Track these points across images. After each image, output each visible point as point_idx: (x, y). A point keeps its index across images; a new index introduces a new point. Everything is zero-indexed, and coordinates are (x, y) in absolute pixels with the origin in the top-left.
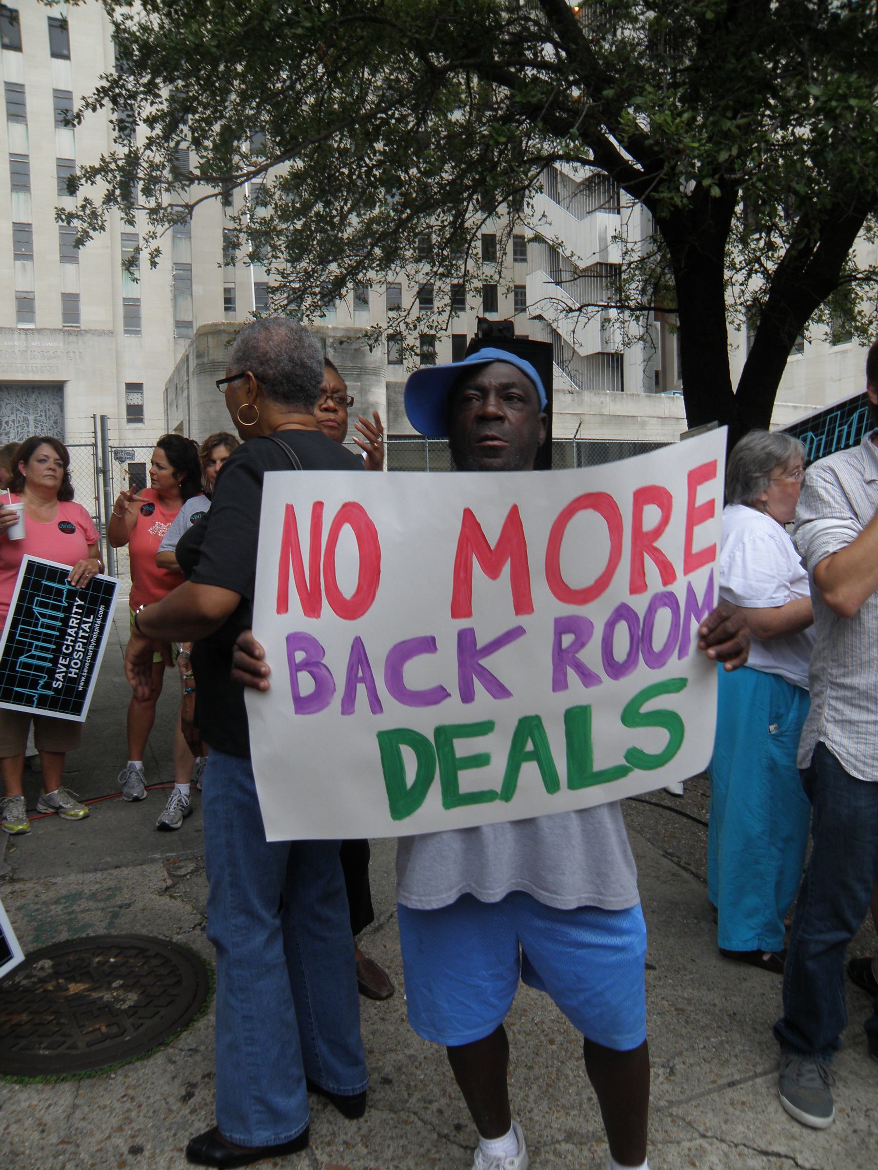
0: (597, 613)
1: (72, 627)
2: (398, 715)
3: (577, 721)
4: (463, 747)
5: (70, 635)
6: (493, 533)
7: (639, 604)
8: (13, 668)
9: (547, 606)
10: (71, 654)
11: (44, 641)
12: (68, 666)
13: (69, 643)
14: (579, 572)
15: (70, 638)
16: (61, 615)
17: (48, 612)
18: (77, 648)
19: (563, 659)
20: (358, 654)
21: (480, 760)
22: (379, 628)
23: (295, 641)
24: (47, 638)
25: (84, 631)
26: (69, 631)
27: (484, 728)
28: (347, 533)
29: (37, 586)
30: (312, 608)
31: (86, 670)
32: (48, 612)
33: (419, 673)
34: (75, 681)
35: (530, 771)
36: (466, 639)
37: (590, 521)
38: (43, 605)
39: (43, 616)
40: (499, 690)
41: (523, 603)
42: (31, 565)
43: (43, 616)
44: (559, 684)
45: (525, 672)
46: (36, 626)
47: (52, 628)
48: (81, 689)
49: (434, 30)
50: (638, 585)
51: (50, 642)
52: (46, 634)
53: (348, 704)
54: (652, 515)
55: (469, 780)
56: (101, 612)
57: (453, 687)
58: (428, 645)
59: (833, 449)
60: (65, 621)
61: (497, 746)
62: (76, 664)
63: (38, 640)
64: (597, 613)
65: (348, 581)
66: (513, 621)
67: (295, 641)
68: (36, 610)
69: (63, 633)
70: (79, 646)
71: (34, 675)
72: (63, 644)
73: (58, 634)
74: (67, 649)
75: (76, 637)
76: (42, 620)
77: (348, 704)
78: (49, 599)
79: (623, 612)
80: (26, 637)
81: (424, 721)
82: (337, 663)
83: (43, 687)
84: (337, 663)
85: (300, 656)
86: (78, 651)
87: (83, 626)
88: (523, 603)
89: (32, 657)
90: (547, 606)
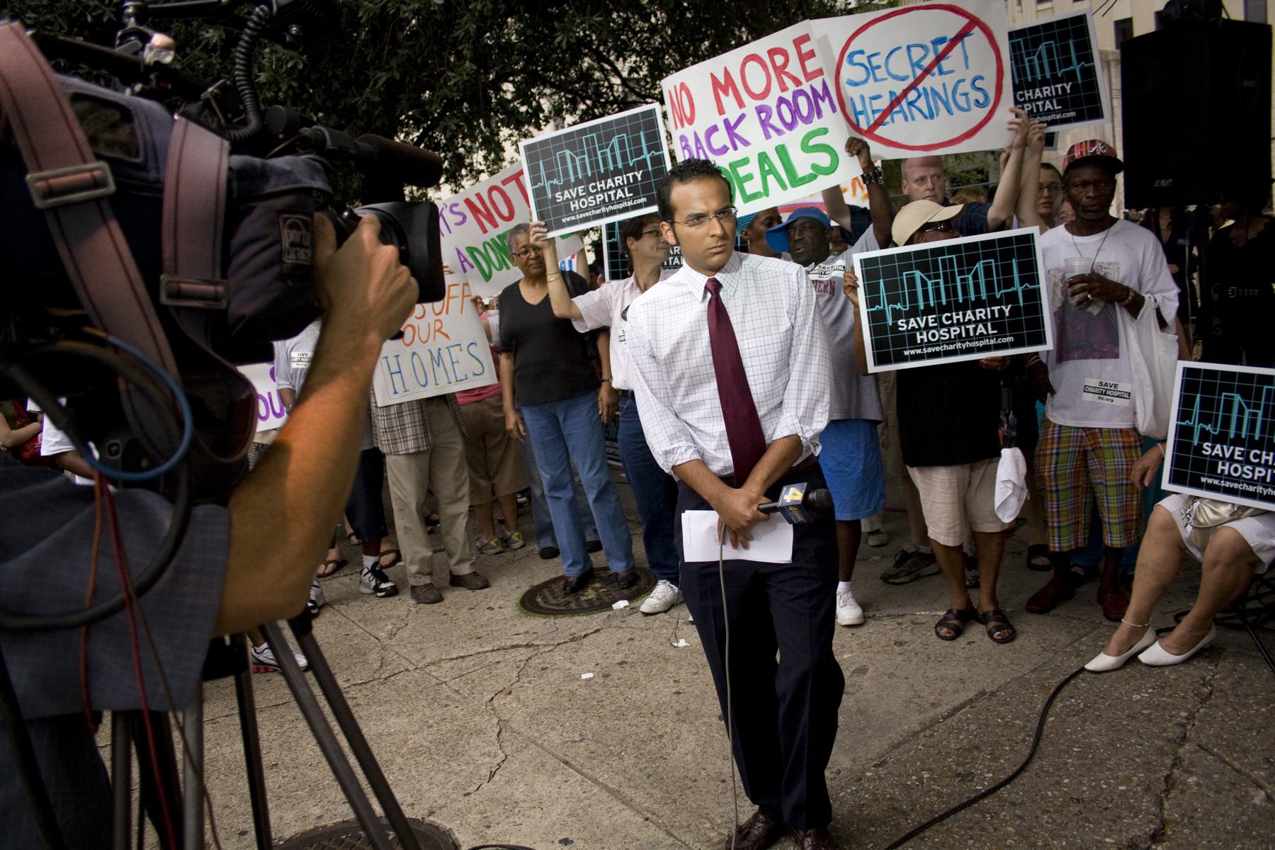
0: (771, 101)
1: (974, 314)
5: (964, 316)
7: (788, 96)
8: (903, 269)
9: (751, 104)
10: (1248, 462)
11: (947, 289)
12: (927, 328)
13: (1264, 457)
15: (960, 316)
16: (984, 296)
17: (982, 280)
18: (1257, 469)
24: (951, 292)
25: (975, 329)
26: (969, 312)
27: (745, 161)
29: (1007, 255)
31: (1228, 484)
32: (982, 280)
34: (1213, 471)
36: (726, 122)
38: (988, 270)
39: (975, 277)
41: (741, 104)
43: (975, 277)
46: (961, 273)
47: (965, 292)
48: (1203, 480)
51: (948, 296)
52: (955, 288)
56: (1005, 340)
57: (729, 145)
58: (714, 129)
60: (979, 303)
61: (753, 168)
62: (934, 336)
63: (946, 282)
68: (979, 266)
69: (963, 307)
70: (955, 331)
71: (904, 294)
72: (1261, 450)
73: (1257, 438)
74: (948, 319)
75: (964, 323)
76: (970, 277)
78: (998, 275)
80: (944, 268)
83: (894, 310)
86: (1253, 471)
87: (980, 326)
88: (741, 104)
89: (924, 284)
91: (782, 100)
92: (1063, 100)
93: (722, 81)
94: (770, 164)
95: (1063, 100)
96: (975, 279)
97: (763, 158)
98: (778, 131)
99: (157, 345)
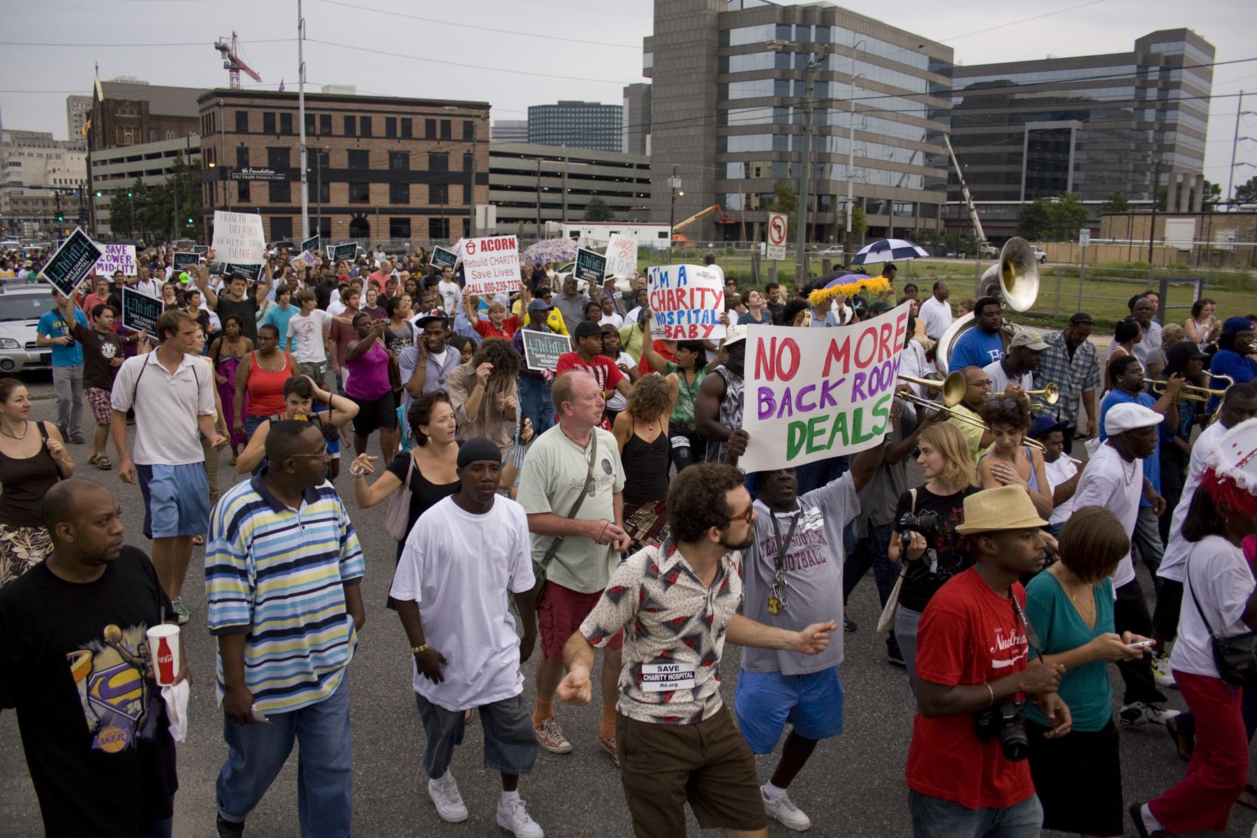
0: (867, 371)
2: (799, 416)
3: (858, 414)
4: (817, 427)
6: (840, 347)
7: (880, 366)
9: (854, 369)
14: (863, 358)
19: (856, 389)
20: (788, 394)
21: (822, 432)
22: (795, 385)
23: (761, 390)
27: (825, 418)
28: (787, 350)
30: (770, 376)
33: (806, 400)
35: (839, 435)
36: (826, 383)
37: (869, 337)
40: (833, 403)
41: (846, 370)
42: (1068, 132)
44: (854, 399)
45: (842, 394)
49: (1047, 175)
50: (880, 360)
53: (780, 415)
54: (886, 333)
55: (817, 441)
57: (818, 404)
58: (813, 388)
59: (855, 524)
61: (828, 426)
64: (867, 371)
65: (786, 366)
66: (842, 376)
67: (761, 390)
77: (780, 415)
79: (876, 370)
81: (804, 417)
82: (778, 398)
84: (778, 398)
85: (763, 396)
88: (846, 370)
90: (854, 369)
91: (876, 370)
92: (88, 259)
93: (840, 348)
94: (844, 424)
95: (88, 259)
96: (74, 252)
97: (841, 417)
98: (863, 396)
99: (299, 547)
